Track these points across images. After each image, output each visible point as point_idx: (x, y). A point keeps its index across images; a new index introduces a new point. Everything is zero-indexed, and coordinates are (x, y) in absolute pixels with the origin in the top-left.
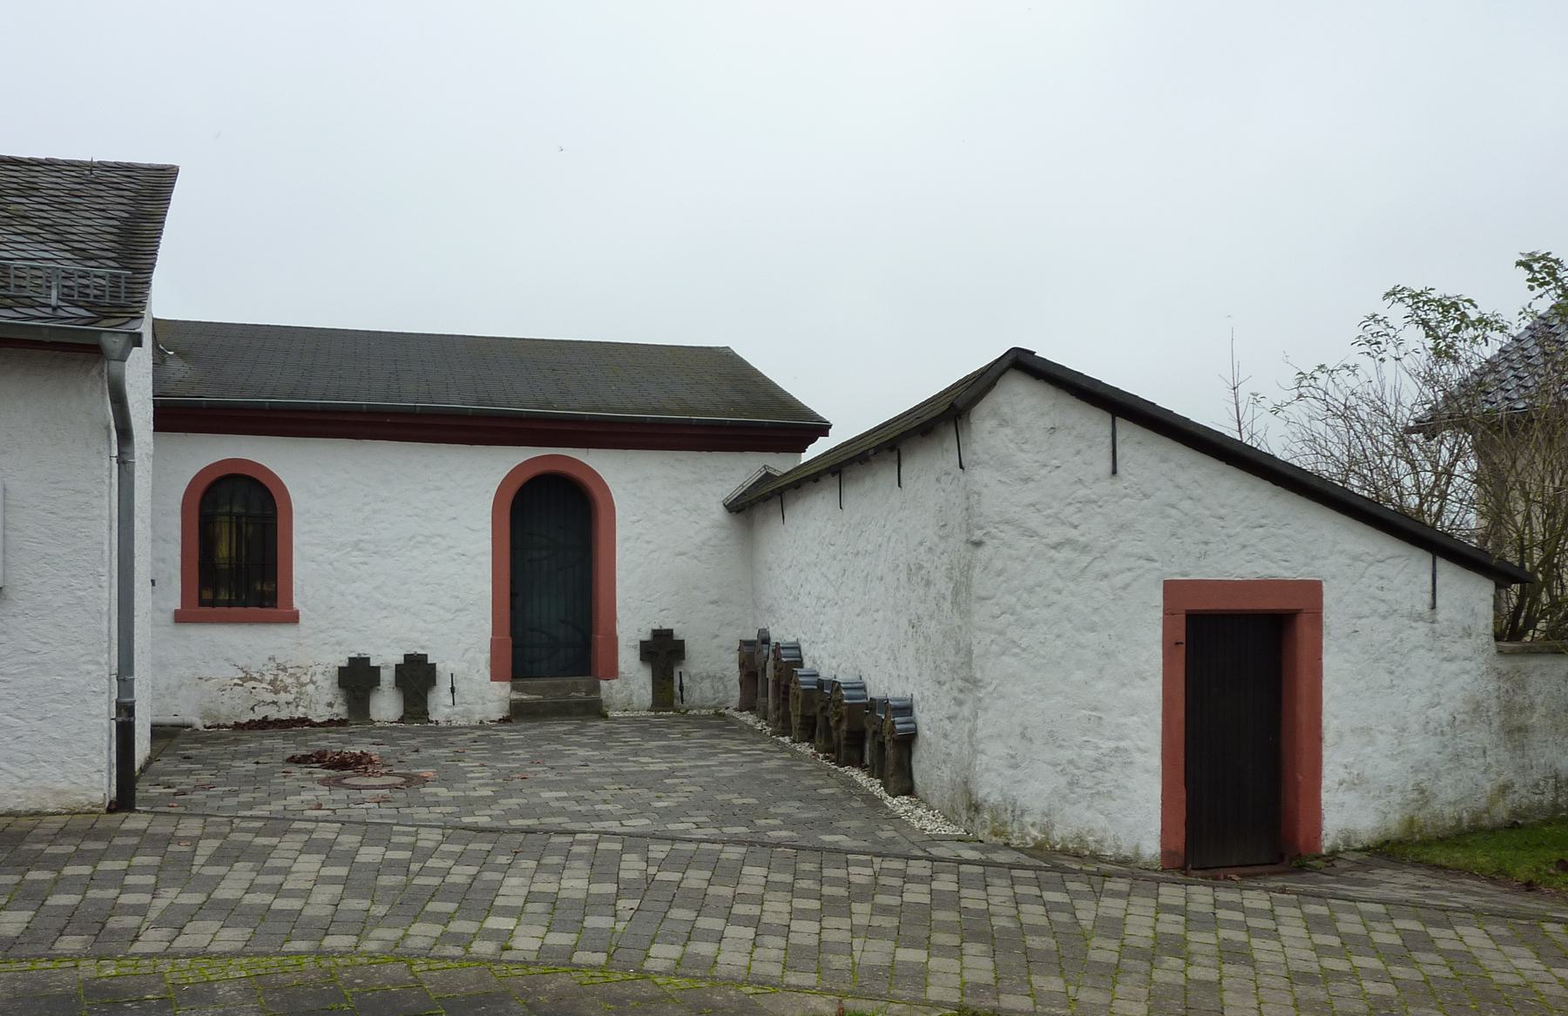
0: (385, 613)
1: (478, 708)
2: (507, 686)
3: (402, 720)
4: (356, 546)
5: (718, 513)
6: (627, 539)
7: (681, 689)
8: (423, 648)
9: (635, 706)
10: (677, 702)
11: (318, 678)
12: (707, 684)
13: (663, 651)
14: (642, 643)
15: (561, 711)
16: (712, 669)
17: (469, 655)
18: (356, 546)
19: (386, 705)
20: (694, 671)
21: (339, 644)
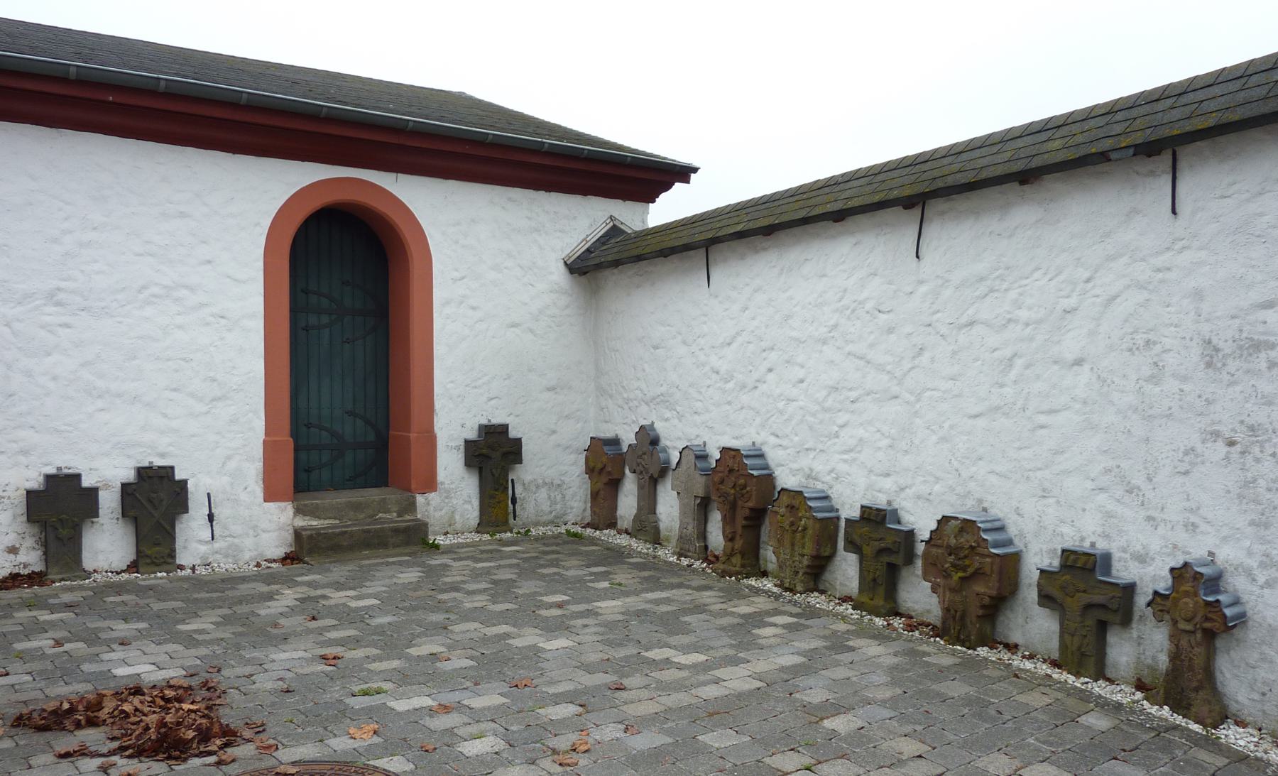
0: (100, 404)
1: (249, 542)
4: (52, 297)
5: (559, 274)
6: (447, 303)
7: (514, 501)
8: (162, 455)
9: (458, 526)
10: (511, 520)
12: (543, 494)
13: (494, 453)
16: (552, 478)
17: (232, 465)
18: (52, 297)
19: (107, 545)
21: (24, 452)
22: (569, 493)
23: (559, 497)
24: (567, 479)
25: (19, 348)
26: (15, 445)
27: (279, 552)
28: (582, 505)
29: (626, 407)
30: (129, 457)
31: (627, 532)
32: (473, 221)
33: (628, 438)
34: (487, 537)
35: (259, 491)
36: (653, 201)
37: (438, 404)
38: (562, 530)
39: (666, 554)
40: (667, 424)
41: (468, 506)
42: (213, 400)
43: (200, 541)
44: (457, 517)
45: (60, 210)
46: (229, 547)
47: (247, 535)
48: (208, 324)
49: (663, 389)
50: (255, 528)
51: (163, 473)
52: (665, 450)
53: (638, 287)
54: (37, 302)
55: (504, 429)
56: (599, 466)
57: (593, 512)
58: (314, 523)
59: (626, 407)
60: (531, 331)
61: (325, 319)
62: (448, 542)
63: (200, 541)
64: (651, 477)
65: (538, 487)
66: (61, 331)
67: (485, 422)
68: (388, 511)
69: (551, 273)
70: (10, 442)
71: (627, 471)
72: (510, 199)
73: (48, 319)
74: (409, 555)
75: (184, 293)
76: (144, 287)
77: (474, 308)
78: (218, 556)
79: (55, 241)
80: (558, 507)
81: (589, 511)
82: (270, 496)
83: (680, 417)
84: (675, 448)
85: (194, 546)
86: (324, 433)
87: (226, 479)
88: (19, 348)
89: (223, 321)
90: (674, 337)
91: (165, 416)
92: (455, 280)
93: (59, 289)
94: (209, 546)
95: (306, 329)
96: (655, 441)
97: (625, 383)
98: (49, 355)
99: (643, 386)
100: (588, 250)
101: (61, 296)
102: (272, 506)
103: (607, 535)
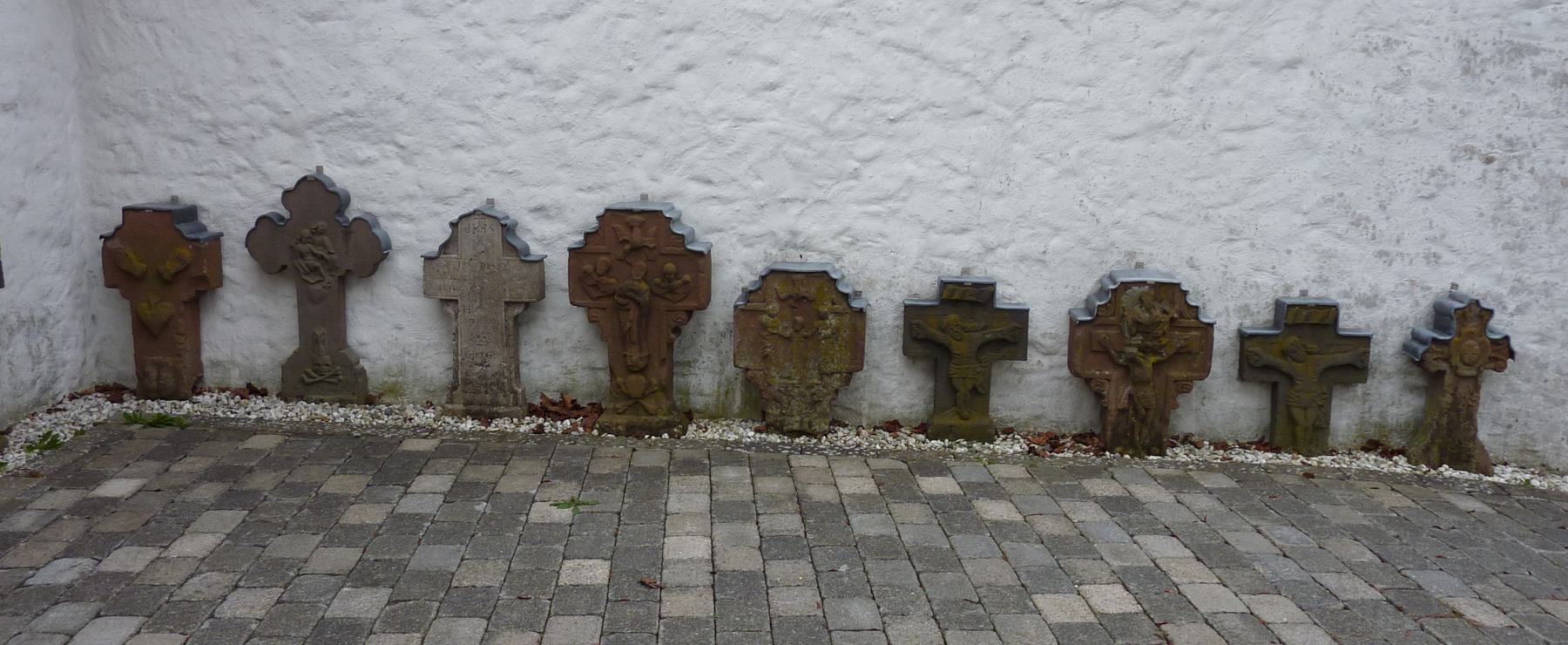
24: (51, 303)
40: (368, 171)
49: (356, 100)
80: (44, 367)
83: (407, 155)
99: (279, 96)
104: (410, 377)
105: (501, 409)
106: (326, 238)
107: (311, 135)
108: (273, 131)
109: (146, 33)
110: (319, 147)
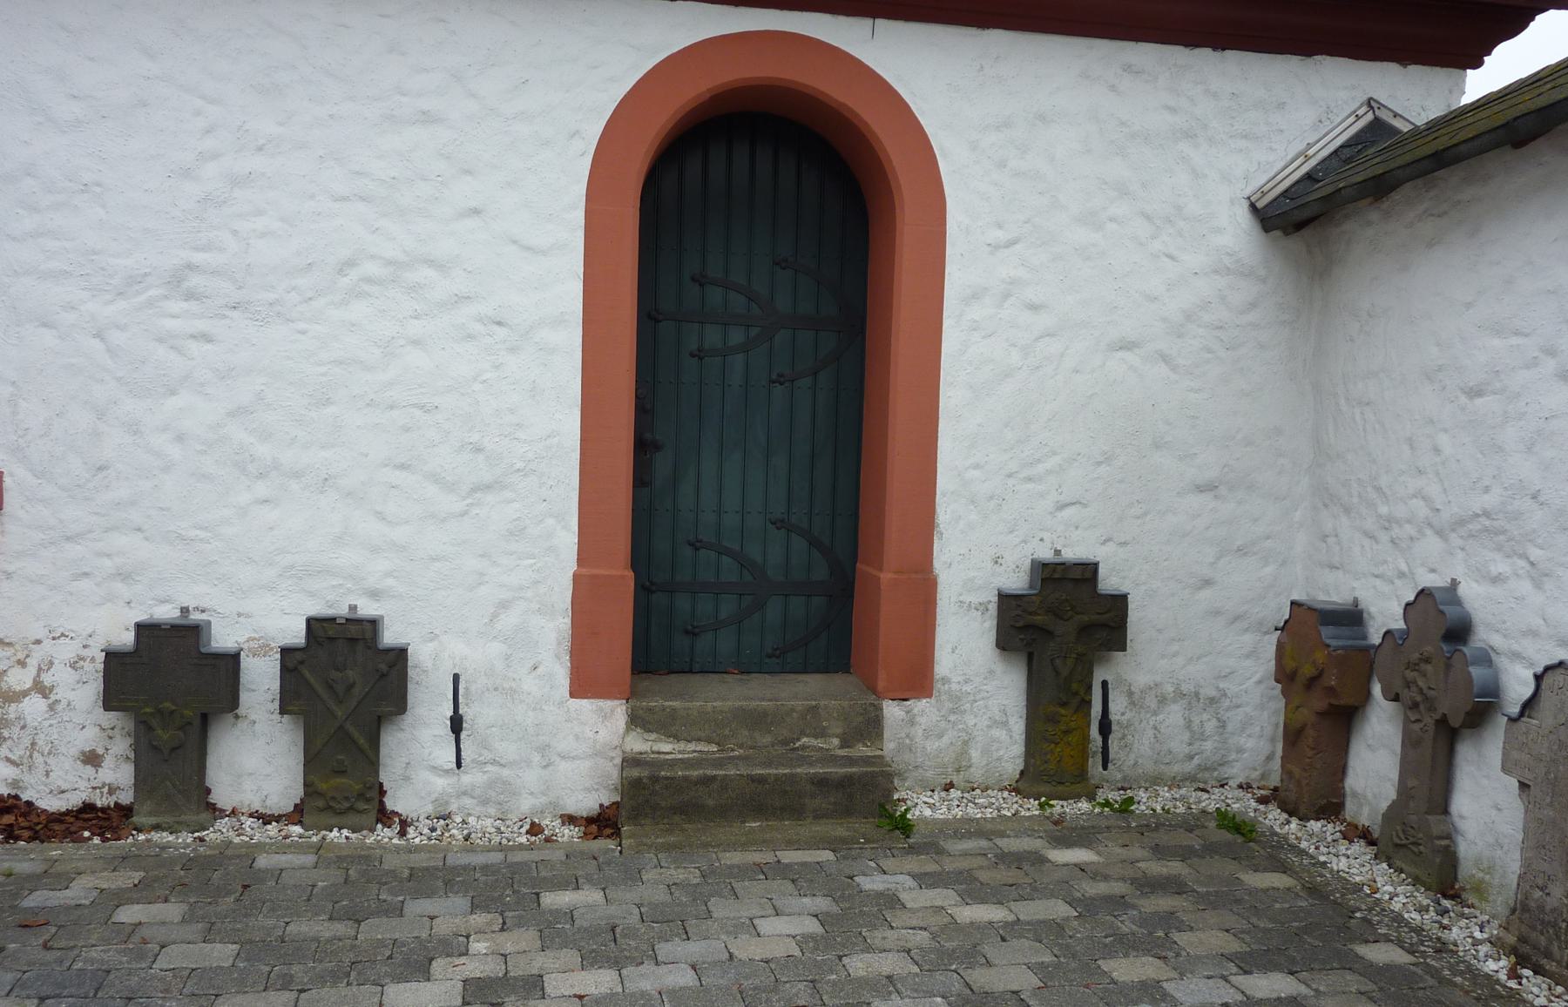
0: (261, 489)
1: (531, 778)
2: (617, 711)
3: (297, 815)
4: (178, 281)
5: (1235, 231)
6: (975, 296)
7: (1105, 728)
8: (375, 594)
9: (977, 774)
10: (1094, 767)
11: (60, 676)
12: (1174, 716)
13: (1064, 623)
14: (1007, 601)
15: (771, 802)
16: (1197, 688)
17: (509, 620)
18: (178, 281)
19: (257, 762)
20: (1140, 679)
21: (124, 576)
22: (1235, 718)
23: (1210, 726)
24: (1230, 687)
25: (119, 379)
26: (107, 563)
27: (587, 802)
28: (1264, 747)
29: (1384, 537)
30: (312, 594)
31: (1366, 836)
32: (1042, 118)
33: (1386, 612)
34: (1031, 808)
35: (561, 675)
36: (1477, 63)
37: (945, 511)
38: (1211, 802)
39: (1472, 937)
40: (1496, 591)
41: (997, 733)
42: (474, 490)
43: (434, 769)
44: (975, 754)
45: (198, 113)
46: (491, 784)
47: (528, 763)
48: (471, 337)
49: (1491, 500)
50: (543, 749)
51: (353, 631)
52: (1485, 658)
53: (1431, 244)
54: (152, 292)
55: (1087, 572)
56: (1308, 671)
57: (1286, 772)
58: (666, 747)
59: (1384, 537)
60: (1165, 358)
61: (737, 336)
62: (941, 814)
63: (434, 769)
64: (1442, 722)
65: (1163, 700)
66: (194, 347)
67: (1046, 554)
68: (822, 734)
69: (1218, 230)
70: (100, 554)
71: (1377, 689)
72: (1128, 68)
73: (170, 324)
74: (833, 845)
75: (425, 274)
76: (351, 263)
77: (1034, 307)
78: (468, 802)
79: (187, 173)
80: (1208, 746)
81: (1276, 765)
82: (580, 688)
83: (1539, 576)
84: (1516, 656)
85: (423, 776)
86: (726, 560)
87: (496, 648)
88: (119, 379)
89: (501, 332)
90: (1534, 363)
91: (381, 516)
92: (995, 247)
93: (190, 267)
94: (452, 780)
95: (699, 355)
96: (1459, 632)
97: (1384, 481)
98: (173, 393)
99: (1434, 490)
100: (1309, 177)
101: (195, 281)
102: (585, 704)
103: (1311, 836)
104: (1496, 881)
105: (1551, 966)
106: (1429, 668)
107: (1455, 540)
108: (1429, 532)
109: (1358, 417)
110: (1460, 555)
